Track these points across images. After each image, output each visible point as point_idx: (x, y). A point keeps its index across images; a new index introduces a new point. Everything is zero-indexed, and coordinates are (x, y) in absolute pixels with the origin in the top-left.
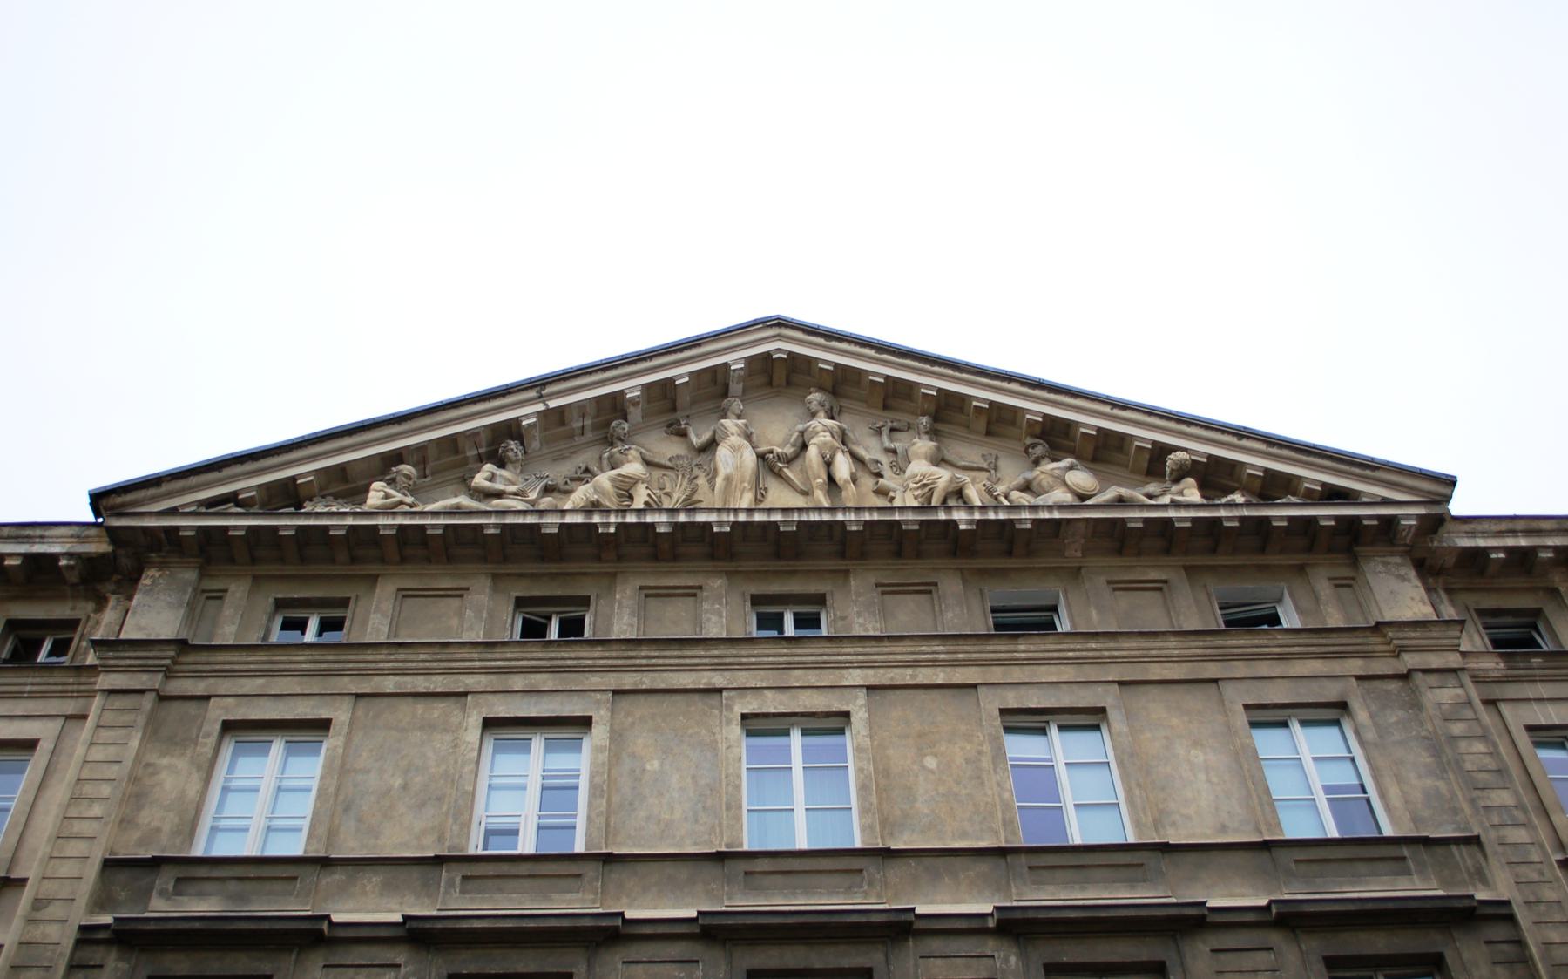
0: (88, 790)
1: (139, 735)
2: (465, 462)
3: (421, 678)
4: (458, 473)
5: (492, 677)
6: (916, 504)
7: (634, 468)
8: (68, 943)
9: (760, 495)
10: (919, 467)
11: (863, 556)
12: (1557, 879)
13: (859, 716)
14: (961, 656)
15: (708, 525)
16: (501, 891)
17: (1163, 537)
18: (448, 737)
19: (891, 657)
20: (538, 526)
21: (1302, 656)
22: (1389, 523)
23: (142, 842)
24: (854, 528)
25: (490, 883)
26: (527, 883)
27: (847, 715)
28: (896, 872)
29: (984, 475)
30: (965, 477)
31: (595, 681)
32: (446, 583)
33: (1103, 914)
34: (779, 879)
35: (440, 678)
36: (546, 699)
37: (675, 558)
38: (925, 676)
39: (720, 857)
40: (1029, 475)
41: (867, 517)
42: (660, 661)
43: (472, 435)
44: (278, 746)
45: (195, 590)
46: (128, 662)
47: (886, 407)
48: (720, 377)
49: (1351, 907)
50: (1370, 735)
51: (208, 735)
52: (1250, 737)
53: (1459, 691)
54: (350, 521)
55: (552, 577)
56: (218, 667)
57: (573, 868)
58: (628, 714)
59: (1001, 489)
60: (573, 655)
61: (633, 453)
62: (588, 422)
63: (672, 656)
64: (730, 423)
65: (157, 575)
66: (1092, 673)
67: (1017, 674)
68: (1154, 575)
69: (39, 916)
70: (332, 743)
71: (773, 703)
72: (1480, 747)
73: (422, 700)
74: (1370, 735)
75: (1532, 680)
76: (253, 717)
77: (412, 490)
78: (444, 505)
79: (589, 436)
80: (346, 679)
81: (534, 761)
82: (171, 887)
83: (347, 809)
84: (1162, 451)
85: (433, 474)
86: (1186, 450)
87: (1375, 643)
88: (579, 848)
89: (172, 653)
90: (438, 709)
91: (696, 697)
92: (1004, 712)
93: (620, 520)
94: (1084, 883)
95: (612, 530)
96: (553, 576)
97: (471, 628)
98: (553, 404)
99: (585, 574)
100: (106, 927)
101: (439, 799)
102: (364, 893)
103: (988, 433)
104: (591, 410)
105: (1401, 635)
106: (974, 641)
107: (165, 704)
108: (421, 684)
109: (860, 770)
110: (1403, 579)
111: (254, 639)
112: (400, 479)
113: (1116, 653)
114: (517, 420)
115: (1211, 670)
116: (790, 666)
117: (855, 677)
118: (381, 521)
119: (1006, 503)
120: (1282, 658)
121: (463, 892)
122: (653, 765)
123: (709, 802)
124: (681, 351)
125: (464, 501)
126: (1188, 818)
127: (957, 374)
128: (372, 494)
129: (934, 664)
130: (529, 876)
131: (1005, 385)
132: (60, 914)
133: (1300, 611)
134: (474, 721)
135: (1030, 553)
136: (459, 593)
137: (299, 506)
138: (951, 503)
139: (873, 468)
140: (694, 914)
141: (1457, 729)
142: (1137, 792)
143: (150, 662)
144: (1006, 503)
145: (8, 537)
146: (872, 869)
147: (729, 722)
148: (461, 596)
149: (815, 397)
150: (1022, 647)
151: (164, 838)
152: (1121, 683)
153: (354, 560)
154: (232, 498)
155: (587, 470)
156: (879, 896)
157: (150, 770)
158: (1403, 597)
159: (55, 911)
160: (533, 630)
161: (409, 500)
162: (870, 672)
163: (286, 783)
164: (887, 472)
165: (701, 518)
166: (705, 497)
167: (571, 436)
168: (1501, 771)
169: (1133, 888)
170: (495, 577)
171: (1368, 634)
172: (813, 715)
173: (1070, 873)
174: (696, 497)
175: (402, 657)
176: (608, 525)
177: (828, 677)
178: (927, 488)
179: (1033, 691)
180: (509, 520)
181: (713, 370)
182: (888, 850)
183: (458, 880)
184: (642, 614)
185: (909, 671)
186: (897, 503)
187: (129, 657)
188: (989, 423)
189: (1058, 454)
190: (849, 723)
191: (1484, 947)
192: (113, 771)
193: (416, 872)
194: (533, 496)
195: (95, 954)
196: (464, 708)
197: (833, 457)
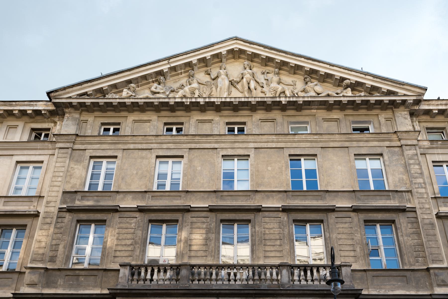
0: (57, 174)
6: (272, 96)
7: (195, 85)
8: (56, 212)
10: (274, 85)
12: (430, 202)
13: (252, 156)
15: (214, 102)
17: (340, 106)
18: (147, 161)
19: (262, 140)
21: (372, 141)
22: (404, 102)
23: (72, 187)
24: (254, 103)
26: (167, 197)
28: (258, 196)
29: (292, 87)
30: (286, 88)
31: (184, 146)
32: (145, 118)
36: (172, 150)
39: (215, 192)
42: (201, 141)
50: (387, 163)
51: (86, 160)
52: (354, 163)
53: (415, 151)
54: (118, 101)
58: (193, 155)
59: (296, 91)
60: (179, 139)
61: (195, 81)
63: (204, 139)
66: (314, 145)
67: (295, 145)
69: (48, 205)
70: (184, 161)
71: (230, 152)
72: (417, 167)
75: (437, 148)
76: (97, 155)
80: (120, 145)
82: (80, 198)
84: (343, 79)
86: (349, 79)
87: (394, 137)
88: (180, 189)
90: (145, 153)
91: (210, 150)
92: (290, 155)
93: (191, 101)
94: (305, 200)
95: (188, 104)
97: (152, 131)
101: (145, 177)
102: (128, 200)
105: (401, 135)
106: (284, 136)
108: (140, 146)
111: (96, 134)
114: (162, 70)
116: (235, 142)
117: (252, 145)
118: (126, 100)
119: (297, 96)
120: (367, 141)
122: (199, 168)
123: (213, 178)
124: (208, 48)
126: (335, 184)
127: (286, 55)
128: (124, 93)
129: (273, 142)
131: (300, 59)
132: (54, 205)
134: (154, 156)
137: (105, 96)
138: (281, 96)
139: (261, 85)
140: (281, 206)
141: (411, 162)
142: (322, 177)
144: (297, 96)
145: (27, 105)
147: (218, 157)
152: (321, 148)
154: (85, 94)
155: (183, 85)
158: (404, 122)
159: (52, 204)
160: (231, 130)
162: (256, 144)
164: (265, 86)
165: (212, 100)
166: (214, 94)
168: (422, 174)
171: (392, 134)
174: (212, 94)
176: (187, 102)
177: (245, 145)
179: (298, 149)
180: (161, 100)
183: (151, 197)
184: (196, 127)
185: (266, 144)
186: (267, 96)
191: (406, 219)
192: (63, 169)
193: (140, 195)
194: (167, 93)
195: (64, 214)
196: (151, 153)
197: (250, 81)
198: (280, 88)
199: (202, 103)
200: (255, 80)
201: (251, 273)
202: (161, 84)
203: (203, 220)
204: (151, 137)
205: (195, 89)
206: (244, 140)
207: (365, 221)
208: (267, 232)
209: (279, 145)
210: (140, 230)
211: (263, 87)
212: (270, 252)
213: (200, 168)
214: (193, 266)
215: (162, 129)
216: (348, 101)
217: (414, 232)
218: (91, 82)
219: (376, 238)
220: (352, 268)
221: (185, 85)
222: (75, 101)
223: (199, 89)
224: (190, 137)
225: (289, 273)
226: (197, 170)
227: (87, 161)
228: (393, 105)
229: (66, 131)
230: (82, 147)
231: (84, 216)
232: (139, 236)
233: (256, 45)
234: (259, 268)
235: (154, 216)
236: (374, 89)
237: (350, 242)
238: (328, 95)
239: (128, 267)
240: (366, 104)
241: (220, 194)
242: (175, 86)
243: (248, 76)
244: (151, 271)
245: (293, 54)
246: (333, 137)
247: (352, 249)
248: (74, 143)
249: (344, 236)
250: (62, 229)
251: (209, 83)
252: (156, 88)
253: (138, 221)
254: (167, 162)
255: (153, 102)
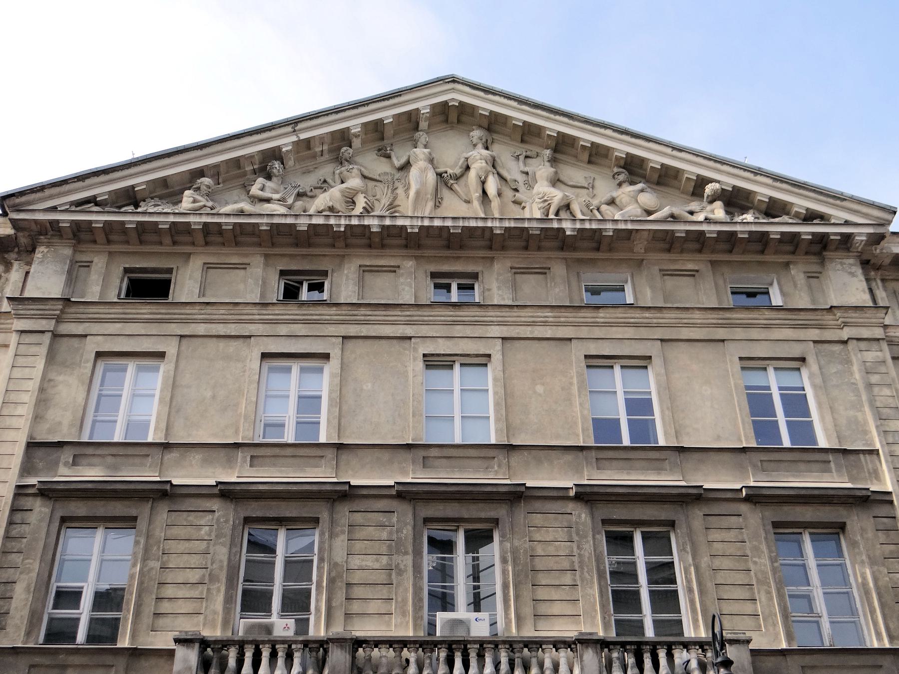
1: (43, 361)
2: (245, 174)
3: (222, 325)
4: (241, 181)
5: (266, 326)
7: (355, 182)
9: (437, 204)
10: (543, 187)
11: (503, 248)
13: (497, 357)
14: (562, 319)
16: (274, 465)
18: (240, 365)
20: (294, 225)
21: (780, 326)
22: (847, 239)
23: (50, 431)
24: (498, 232)
25: (268, 460)
26: (290, 460)
27: (489, 356)
29: (584, 191)
30: (570, 193)
32: (235, 260)
33: (640, 491)
34: (444, 461)
35: (233, 326)
36: (301, 340)
37: (383, 246)
38: (539, 332)
39: (409, 447)
40: (615, 194)
41: (507, 224)
43: (250, 157)
44: (100, 533)
45: (71, 261)
46: (32, 312)
47: (522, 141)
48: (413, 119)
49: (792, 492)
51: (87, 361)
53: (879, 353)
54: (172, 219)
55: (302, 260)
56: (90, 316)
57: (319, 452)
60: (317, 312)
61: (355, 171)
62: (326, 147)
64: (420, 152)
65: (46, 250)
66: (644, 333)
67: (598, 332)
68: (690, 266)
70: (165, 368)
71: (442, 347)
73: (222, 339)
74: (819, 381)
77: (209, 195)
78: (231, 208)
79: (327, 156)
81: (293, 381)
82: (71, 460)
83: (178, 411)
84: (702, 182)
85: (224, 182)
86: (718, 182)
89: (61, 307)
90: (233, 346)
91: (395, 341)
93: (348, 223)
95: (342, 229)
96: (304, 256)
98: (303, 136)
99: (324, 255)
100: (34, 486)
102: (191, 465)
103: (590, 162)
104: (328, 140)
105: (846, 315)
106: (571, 310)
107: (57, 338)
108: (221, 329)
109: (495, 393)
110: (853, 275)
112: (203, 188)
113: (661, 321)
114: (279, 148)
115: (721, 333)
116: (455, 323)
118: (192, 219)
120: (767, 327)
121: (251, 466)
122: (368, 386)
124: (388, 99)
125: (246, 206)
127: (571, 122)
128: (185, 199)
129: (545, 324)
130: (293, 456)
131: (602, 131)
133: (783, 294)
135: (610, 250)
136: (244, 266)
137: (137, 206)
143: (46, 312)
146: (501, 457)
147: (415, 359)
148: (245, 269)
149: (477, 134)
150: (601, 315)
151: (65, 429)
152: (662, 340)
153: (175, 243)
154: (92, 200)
155: (325, 181)
156: (504, 474)
157: (52, 383)
158: (847, 286)
160: (291, 293)
161: (210, 204)
163: (137, 392)
164: (522, 188)
165: (400, 222)
167: (314, 157)
169: (659, 474)
170: (266, 256)
171: (825, 313)
172: (468, 355)
173: (621, 463)
174: (396, 203)
175: (209, 311)
176: (339, 225)
177: (479, 331)
178: (546, 203)
179: (606, 344)
180: (276, 220)
181: (409, 114)
182: (511, 445)
183: (249, 459)
184: (361, 284)
185: (529, 328)
186: (527, 216)
187: (33, 309)
188: (590, 156)
189: (635, 179)
190: (490, 361)
191: (872, 519)
193: (222, 452)
194: (290, 201)
195: (28, 502)
197: (486, 178)
198: (557, 196)
199: (374, 230)
200: (498, 174)
201: (489, 646)
202: (274, 179)
203: (381, 518)
204: (249, 307)
205: (356, 192)
206: (477, 318)
207: (776, 525)
208: (539, 551)
209: (562, 332)
210: (223, 544)
211: (516, 190)
212: (548, 603)
213: (370, 385)
214: (358, 643)
215: (276, 290)
216: (719, 233)
217: (891, 552)
218: (108, 173)
219: (804, 566)
220: (752, 646)
221: (329, 180)
222: (64, 217)
223: (365, 192)
224: (344, 311)
225: (600, 662)
226: (362, 389)
227: (90, 365)
228: (822, 243)
229: (38, 288)
230: (78, 329)
231: (79, 509)
232: (221, 561)
233: (500, 96)
234: (526, 646)
235: (256, 509)
236: (774, 209)
237: (740, 578)
238: (674, 218)
239: (197, 645)
240: (761, 240)
241: (422, 453)
242: (307, 182)
243: (478, 166)
244: (254, 655)
245: (587, 121)
246: (687, 316)
247: (747, 595)
248: (59, 320)
249: (726, 563)
250: (25, 540)
251: (390, 178)
252: (262, 189)
253: (218, 520)
254: (289, 370)
255: (257, 225)
